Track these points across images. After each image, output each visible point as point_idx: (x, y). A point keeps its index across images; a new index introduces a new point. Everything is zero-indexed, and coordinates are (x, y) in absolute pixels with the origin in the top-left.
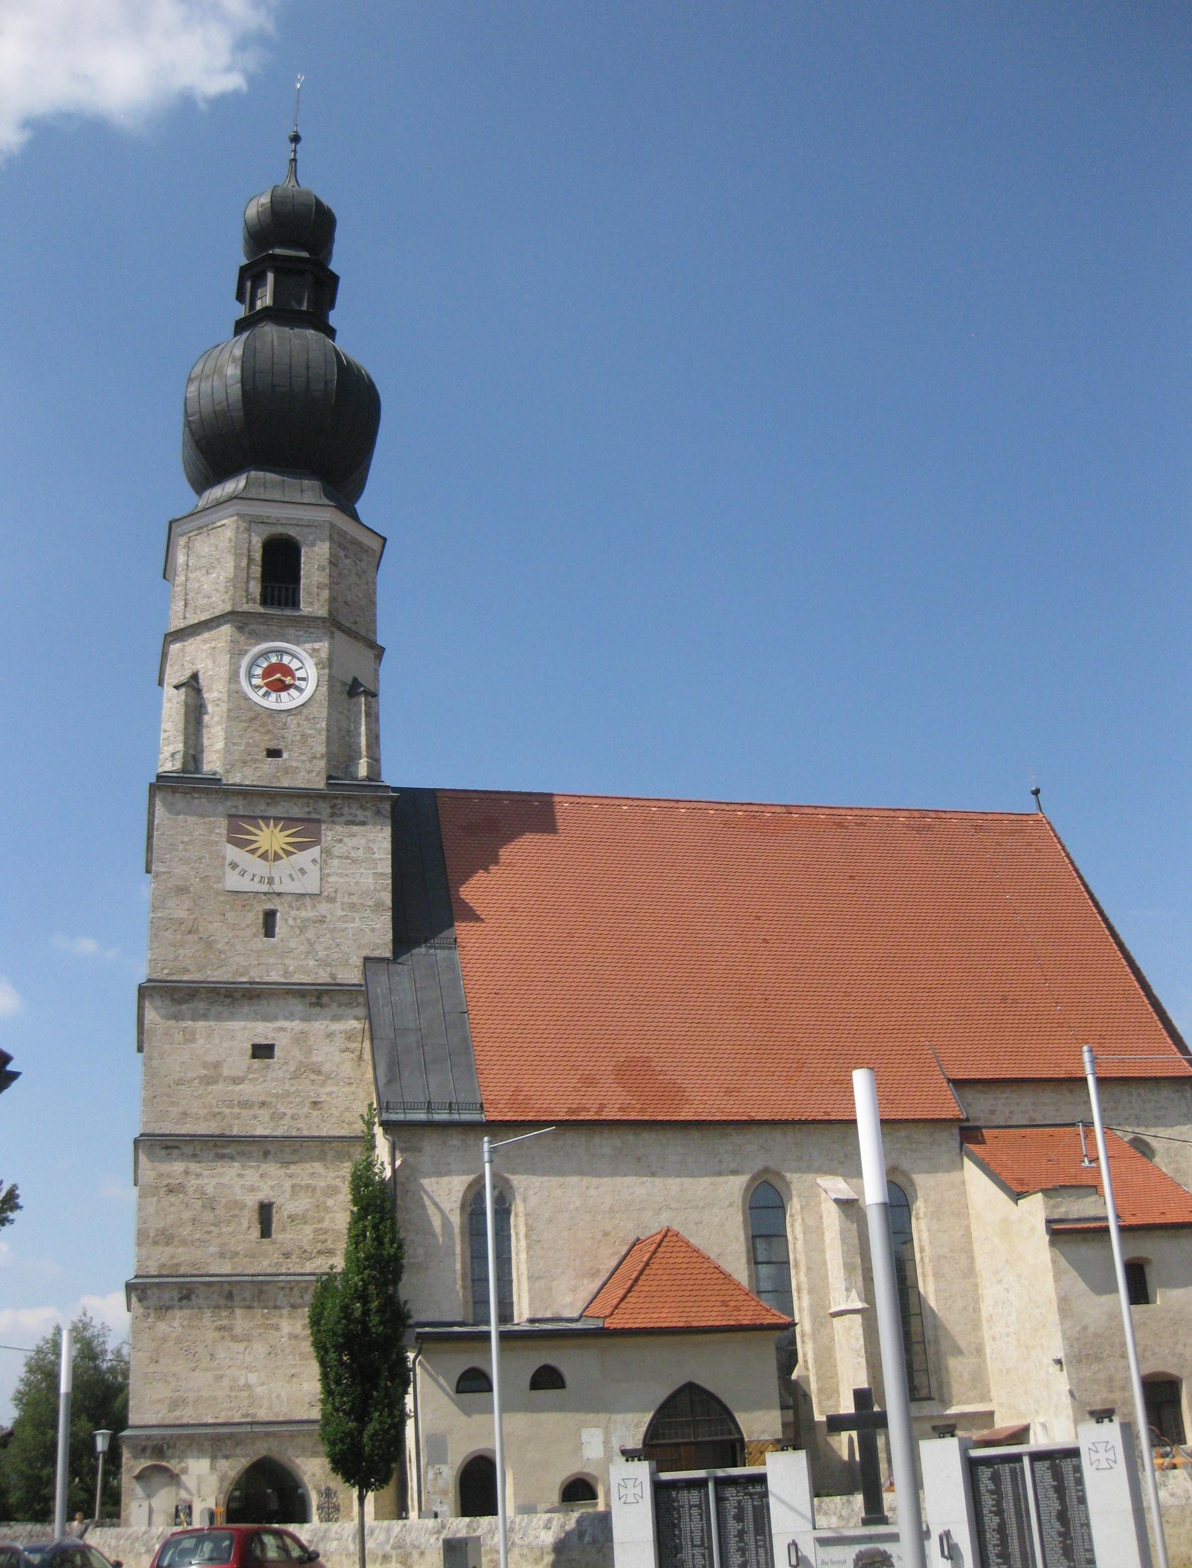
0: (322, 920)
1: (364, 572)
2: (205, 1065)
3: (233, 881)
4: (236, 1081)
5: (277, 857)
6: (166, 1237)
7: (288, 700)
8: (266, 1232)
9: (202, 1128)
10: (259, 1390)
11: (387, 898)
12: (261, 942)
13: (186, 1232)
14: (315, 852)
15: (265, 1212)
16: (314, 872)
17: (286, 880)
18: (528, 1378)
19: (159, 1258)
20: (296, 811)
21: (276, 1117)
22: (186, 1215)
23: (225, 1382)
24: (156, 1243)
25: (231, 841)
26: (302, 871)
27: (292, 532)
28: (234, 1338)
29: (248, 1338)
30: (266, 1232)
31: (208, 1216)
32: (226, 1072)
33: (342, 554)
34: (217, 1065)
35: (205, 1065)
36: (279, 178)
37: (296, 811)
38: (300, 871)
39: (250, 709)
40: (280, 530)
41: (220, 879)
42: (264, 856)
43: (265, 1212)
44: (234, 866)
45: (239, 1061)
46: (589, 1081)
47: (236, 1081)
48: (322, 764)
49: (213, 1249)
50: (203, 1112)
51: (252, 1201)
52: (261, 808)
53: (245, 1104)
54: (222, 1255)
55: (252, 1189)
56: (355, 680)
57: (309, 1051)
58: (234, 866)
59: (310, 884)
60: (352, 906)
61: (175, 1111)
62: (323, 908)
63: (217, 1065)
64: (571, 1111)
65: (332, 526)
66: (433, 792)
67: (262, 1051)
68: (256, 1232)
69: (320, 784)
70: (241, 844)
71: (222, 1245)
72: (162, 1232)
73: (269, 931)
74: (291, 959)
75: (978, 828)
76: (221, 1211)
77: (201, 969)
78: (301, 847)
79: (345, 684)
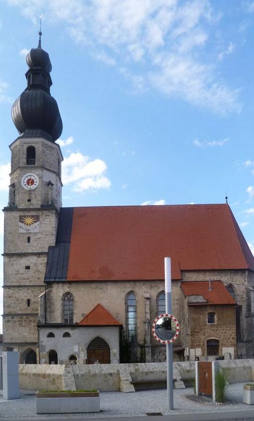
0: (40, 238)
1: (53, 154)
2: (16, 271)
3: (21, 231)
4: (23, 274)
5: (30, 225)
6: (9, 306)
7: (33, 187)
8: (29, 305)
9: (15, 284)
10: (27, 336)
11: (55, 233)
12: (27, 244)
13: (13, 306)
14: (38, 223)
15: (29, 301)
16: (38, 227)
17: (32, 230)
18: (62, 335)
19: (8, 310)
20: (34, 213)
21: (31, 281)
22: (13, 302)
23: (21, 335)
24: (7, 307)
25: (20, 221)
26: (35, 227)
27: (33, 145)
28: (22, 326)
29: (25, 326)
30: (29, 305)
31: (17, 302)
32: (20, 272)
33: (46, 149)
34: (18, 271)
35: (16, 271)
36: (36, 47)
37: (34, 213)
38: (35, 228)
39: (23, 190)
40: (30, 145)
41: (18, 230)
42: (27, 225)
43: (29, 301)
44: (21, 227)
45: (23, 270)
46: (93, 272)
47: (23, 274)
48: (40, 202)
49: (18, 309)
50: (15, 281)
51: (26, 299)
52: (26, 213)
53: (24, 279)
54: (20, 310)
55: (26, 296)
56: (50, 181)
57: (37, 268)
58: (21, 227)
59: (36, 230)
60: (46, 235)
61: (10, 281)
62: (40, 236)
63: (18, 271)
64: (99, 278)
65: (43, 142)
66: (73, 208)
67: (28, 268)
68: (27, 305)
69: (40, 207)
70: (22, 222)
71: (20, 308)
72: (8, 305)
73: (29, 241)
74: (34, 247)
75: (208, 209)
76: (20, 301)
77: (15, 250)
78: (35, 222)
79: (46, 183)
